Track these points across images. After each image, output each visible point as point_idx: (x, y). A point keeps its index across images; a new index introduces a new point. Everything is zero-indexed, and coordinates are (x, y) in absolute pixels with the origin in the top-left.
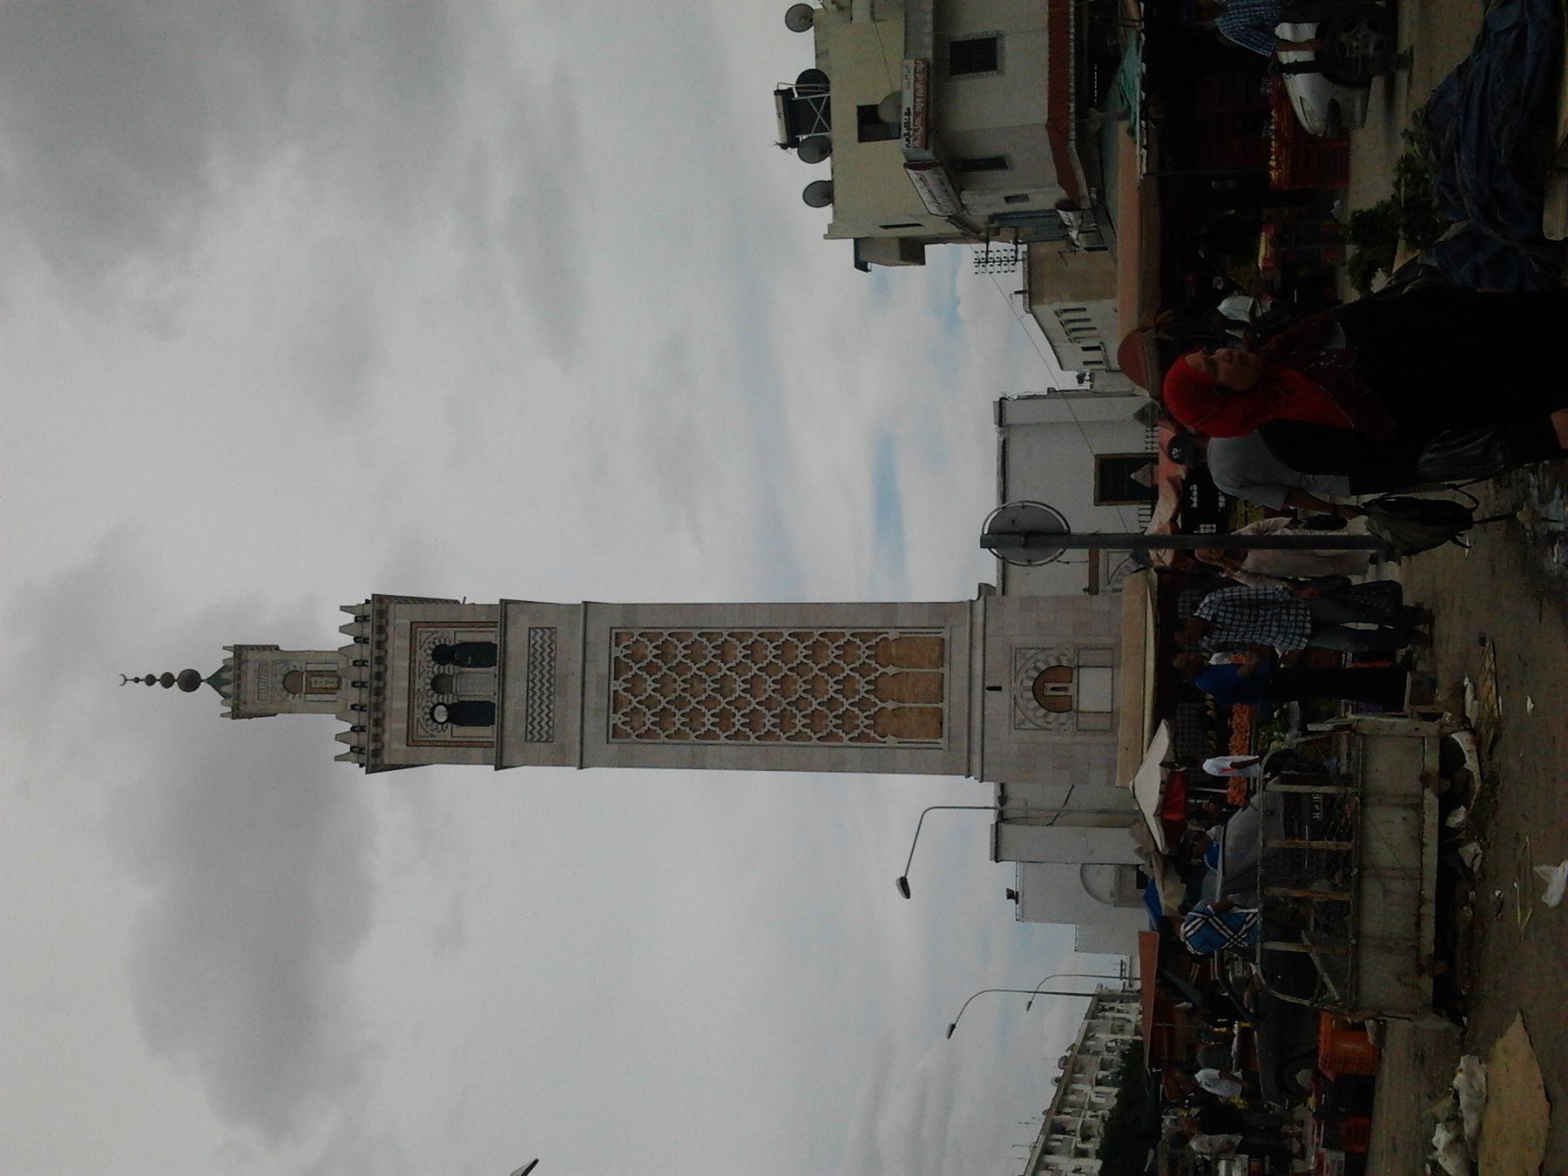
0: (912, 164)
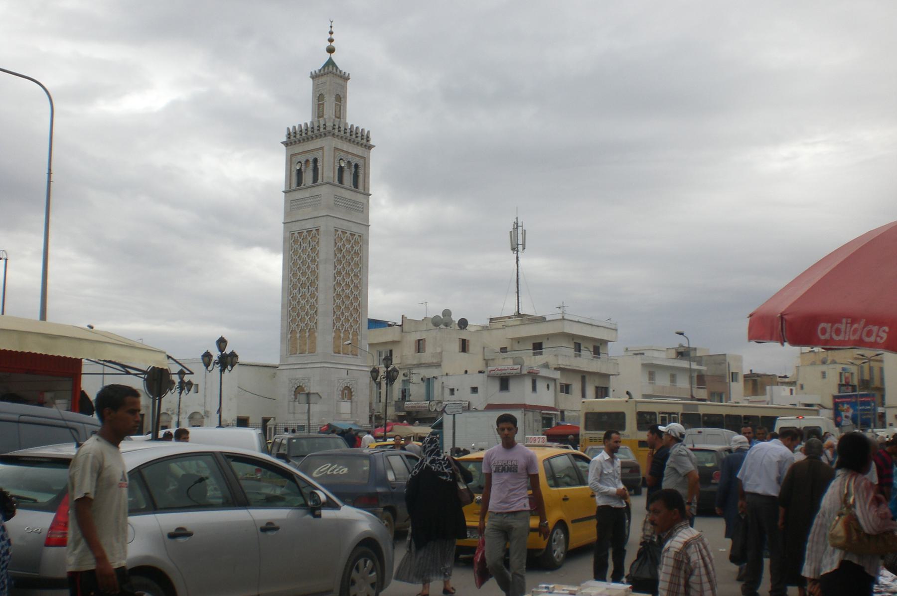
0: (695, 349)
